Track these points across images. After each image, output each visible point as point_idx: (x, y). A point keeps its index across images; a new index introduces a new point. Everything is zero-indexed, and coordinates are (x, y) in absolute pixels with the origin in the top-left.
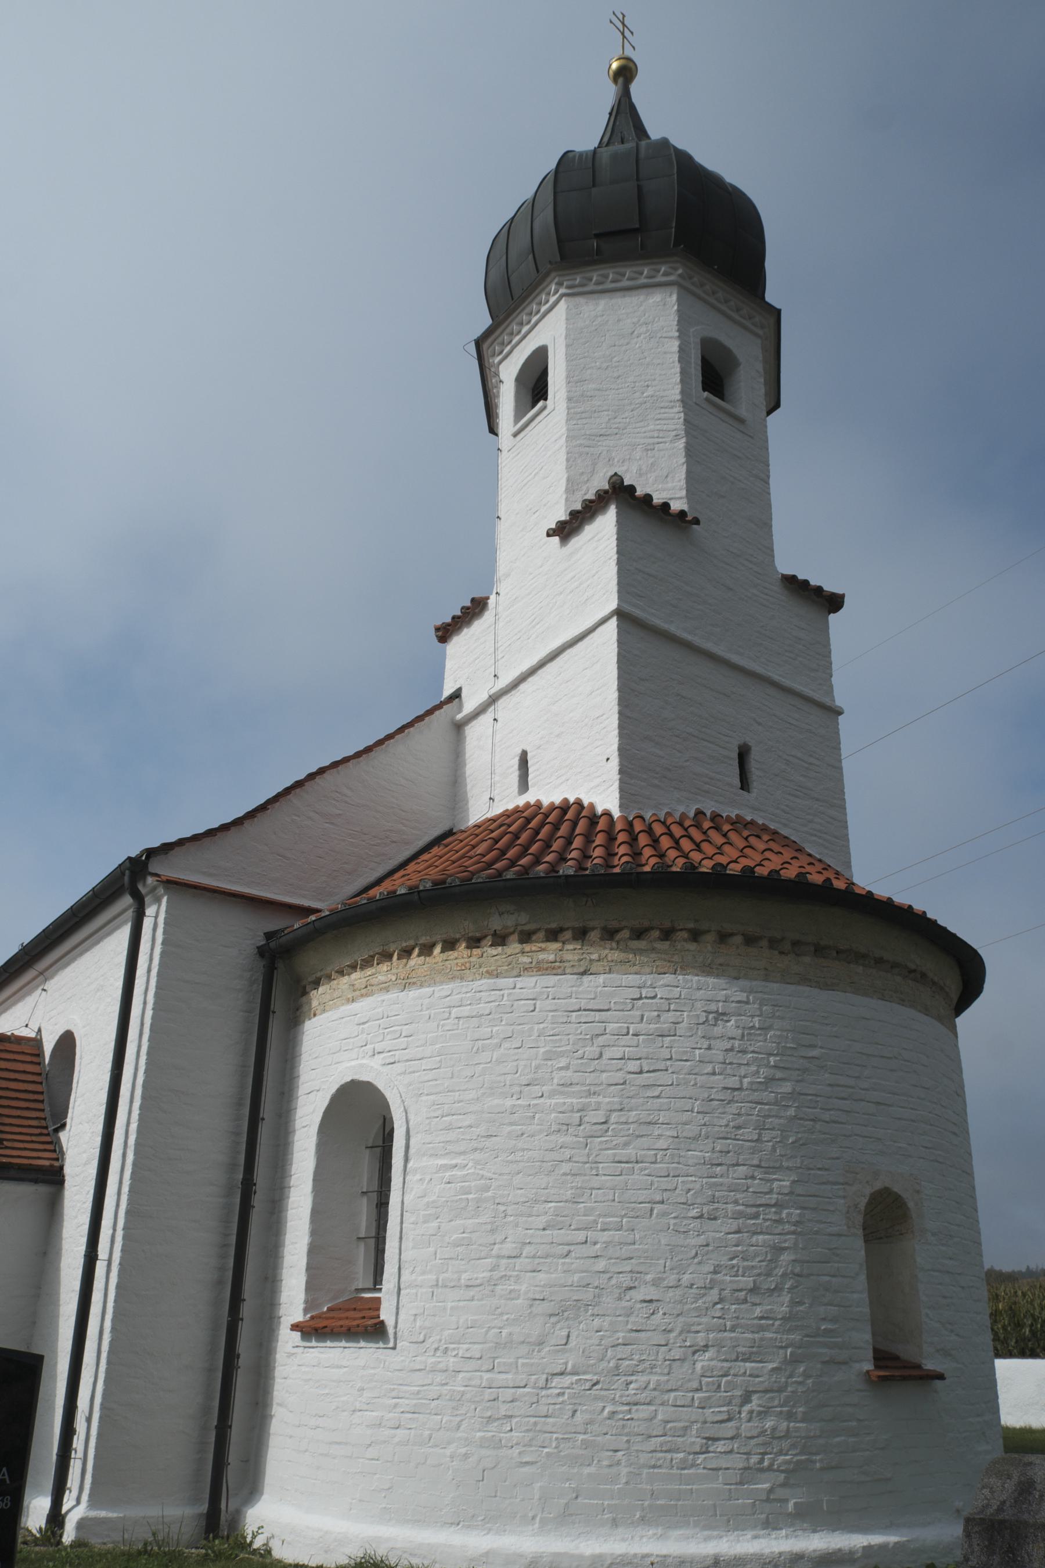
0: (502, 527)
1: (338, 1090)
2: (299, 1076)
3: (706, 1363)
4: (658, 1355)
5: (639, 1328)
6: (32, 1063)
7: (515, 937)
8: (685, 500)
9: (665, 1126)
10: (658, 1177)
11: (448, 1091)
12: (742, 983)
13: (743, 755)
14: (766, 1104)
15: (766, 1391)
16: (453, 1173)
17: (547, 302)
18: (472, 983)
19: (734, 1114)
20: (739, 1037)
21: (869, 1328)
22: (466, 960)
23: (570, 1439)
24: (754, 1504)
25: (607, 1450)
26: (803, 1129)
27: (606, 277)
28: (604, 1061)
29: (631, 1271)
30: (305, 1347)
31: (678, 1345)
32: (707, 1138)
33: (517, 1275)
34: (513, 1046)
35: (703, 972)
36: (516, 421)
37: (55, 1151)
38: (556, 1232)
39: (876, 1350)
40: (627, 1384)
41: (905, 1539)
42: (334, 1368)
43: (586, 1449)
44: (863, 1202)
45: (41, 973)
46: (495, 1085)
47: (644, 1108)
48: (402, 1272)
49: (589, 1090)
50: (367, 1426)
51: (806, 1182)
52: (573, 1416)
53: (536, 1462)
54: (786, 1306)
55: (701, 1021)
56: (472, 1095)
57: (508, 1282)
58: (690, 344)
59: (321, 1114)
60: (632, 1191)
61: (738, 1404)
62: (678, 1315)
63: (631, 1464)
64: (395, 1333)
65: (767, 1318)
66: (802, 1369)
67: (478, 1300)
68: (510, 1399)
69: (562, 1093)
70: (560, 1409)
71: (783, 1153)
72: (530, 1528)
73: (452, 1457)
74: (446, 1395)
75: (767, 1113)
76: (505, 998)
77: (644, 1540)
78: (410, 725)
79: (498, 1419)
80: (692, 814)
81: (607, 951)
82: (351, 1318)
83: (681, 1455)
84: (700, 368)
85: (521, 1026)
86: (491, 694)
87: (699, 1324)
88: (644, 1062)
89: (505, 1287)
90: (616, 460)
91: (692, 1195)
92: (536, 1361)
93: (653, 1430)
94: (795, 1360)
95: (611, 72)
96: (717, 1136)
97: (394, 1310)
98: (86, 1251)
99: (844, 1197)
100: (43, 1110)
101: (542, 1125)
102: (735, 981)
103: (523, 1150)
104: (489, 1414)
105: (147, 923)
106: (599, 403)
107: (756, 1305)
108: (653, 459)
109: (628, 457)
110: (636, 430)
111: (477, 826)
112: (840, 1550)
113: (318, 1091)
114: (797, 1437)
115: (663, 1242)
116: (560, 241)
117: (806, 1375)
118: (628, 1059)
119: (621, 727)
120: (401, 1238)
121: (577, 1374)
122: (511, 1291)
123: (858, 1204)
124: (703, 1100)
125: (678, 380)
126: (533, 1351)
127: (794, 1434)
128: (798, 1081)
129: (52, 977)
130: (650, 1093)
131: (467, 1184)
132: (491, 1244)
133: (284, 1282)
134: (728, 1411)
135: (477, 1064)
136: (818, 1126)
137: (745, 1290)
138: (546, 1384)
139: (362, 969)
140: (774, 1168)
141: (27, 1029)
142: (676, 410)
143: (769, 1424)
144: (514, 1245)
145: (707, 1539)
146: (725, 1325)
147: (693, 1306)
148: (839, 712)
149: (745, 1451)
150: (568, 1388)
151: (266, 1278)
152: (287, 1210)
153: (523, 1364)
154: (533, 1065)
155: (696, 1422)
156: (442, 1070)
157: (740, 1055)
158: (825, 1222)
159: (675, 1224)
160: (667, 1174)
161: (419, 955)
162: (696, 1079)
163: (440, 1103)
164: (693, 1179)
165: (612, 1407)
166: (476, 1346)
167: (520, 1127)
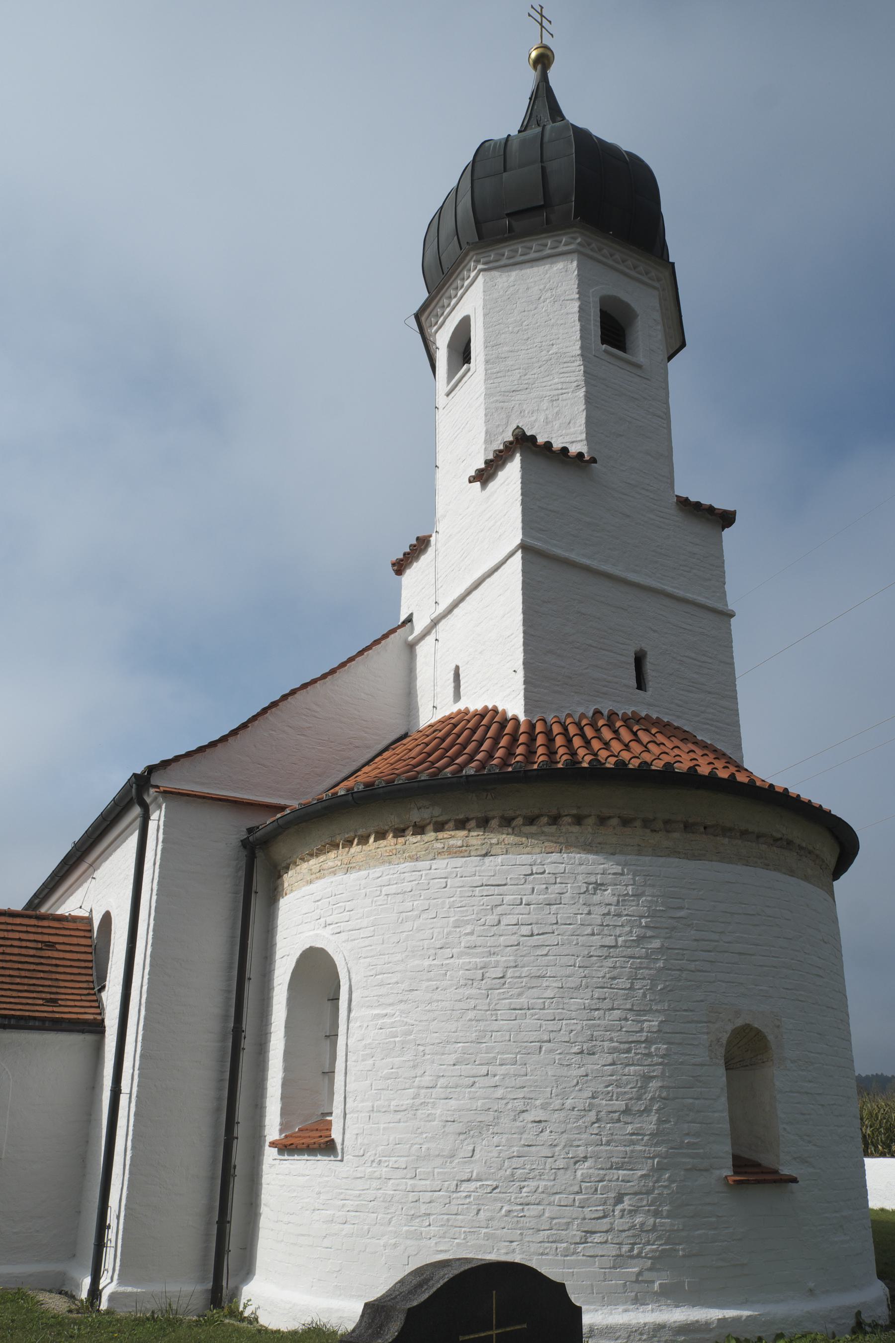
0: (440, 474)
1: (301, 955)
2: (276, 944)
3: (585, 1171)
4: (545, 1165)
5: (530, 1144)
6: (85, 937)
7: (430, 827)
8: (585, 442)
9: (551, 979)
10: (545, 1020)
11: (380, 955)
12: (621, 858)
13: (639, 661)
14: (639, 958)
15: (635, 1194)
16: (385, 1020)
17: (469, 277)
18: (397, 866)
19: (610, 968)
20: (615, 904)
21: (729, 1141)
22: (393, 847)
23: (475, 1232)
24: (625, 1285)
26: (671, 978)
28: (502, 927)
29: (524, 1098)
30: (281, 1160)
31: (562, 1156)
33: (434, 1102)
34: (430, 917)
35: (584, 850)
37: (99, 1007)
38: (464, 1067)
39: (735, 1158)
40: (521, 1188)
41: (757, 1313)
42: (299, 1176)
43: (488, 1240)
44: (725, 1038)
45: (91, 865)
46: (416, 949)
47: (535, 964)
48: (347, 1100)
50: (323, 1222)
51: (673, 1022)
52: (477, 1214)
53: (449, 1251)
54: (655, 1124)
55: (582, 891)
56: (399, 957)
57: (427, 1107)
58: (590, 303)
59: (290, 975)
61: (612, 1204)
62: (562, 1133)
63: (524, 1252)
64: (343, 1149)
65: (637, 1134)
66: (667, 1176)
68: (429, 1201)
69: (468, 954)
70: (467, 1208)
73: (385, 1246)
74: (380, 1198)
75: (638, 966)
76: (423, 878)
78: (368, 648)
80: (590, 714)
81: (504, 836)
82: (312, 1137)
83: (565, 1245)
84: (599, 324)
85: (435, 901)
86: (432, 618)
87: (580, 1140)
88: (535, 927)
89: (424, 1111)
90: (526, 412)
91: (574, 1035)
92: (449, 1170)
93: (542, 1225)
94: (661, 1168)
95: (531, 62)
97: (341, 1130)
98: (112, 1087)
99: (708, 1033)
100: (92, 975)
101: (452, 980)
102: (612, 856)
103: (438, 1001)
104: (412, 1212)
105: (152, 826)
106: (511, 363)
107: (628, 1123)
108: (558, 409)
109: (537, 408)
110: (544, 384)
112: (697, 1321)
113: (288, 955)
114: (663, 1231)
115: (550, 1073)
116: (477, 222)
117: (671, 1180)
118: (522, 925)
119: (525, 644)
120: (346, 1073)
121: (481, 1180)
123: (720, 1038)
124: (584, 957)
125: (579, 337)
126: (446, 1162)
127: (659, 1228)
129: (98, 868)
130: (539, 952)
131: (394, 1029)
132: (413, 1077)
133: (267, 1108)
134: (604, 1210)
135: (401, 932)
136: (684, 975)
137: (619, 1111)
138: (457, 1188)
139: (317, 856)
140: (644, 1010)
141: (81, 910)
143: (638, 1220)
144: (431, 1078)
146: (601, 1140)
147: (575, 1125)
148: (731, 615)
149: (618, 1242)
150: (474, 1192)
151: (256, 1105)
152: (269, 1051)
153: (438, 1173)
154: (445, 931)
155: (576, 1218)
156: (375, 938)
157: (616, 918)
158: (689, 1055)
159: (559, 1059)
160: (553, 1018)
161: (358, 845)
162: (577, 939)
163: (374, 964)
164: (575, 1021)
165: (508, 1206)
166: (402, 1159)
167: (435, 983)
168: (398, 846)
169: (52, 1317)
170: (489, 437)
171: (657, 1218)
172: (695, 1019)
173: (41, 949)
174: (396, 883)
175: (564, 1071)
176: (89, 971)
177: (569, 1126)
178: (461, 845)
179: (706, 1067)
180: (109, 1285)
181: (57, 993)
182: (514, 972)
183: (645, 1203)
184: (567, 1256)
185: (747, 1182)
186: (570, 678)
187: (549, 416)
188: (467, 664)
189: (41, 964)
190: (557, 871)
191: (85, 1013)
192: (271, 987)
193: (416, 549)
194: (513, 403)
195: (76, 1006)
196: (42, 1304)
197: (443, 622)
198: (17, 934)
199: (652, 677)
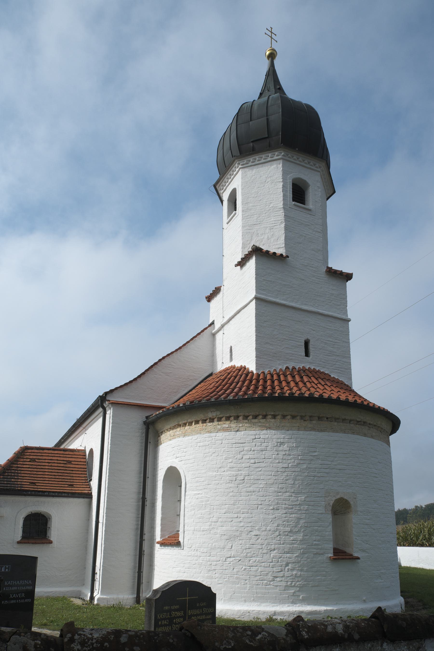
0: (225, 259)
1: (167, 469)
3: (274, 554)
5: (253, 544)
8: (284, 248)
12: (290, 432)
13: (307, 343)
14: (297, 472)
15: (293, 563)
17: (235, 171)
21: (332, 543)
22: (202, 427)
24: (288, 597)
25: (243, 580)
27: (256, 159)
28: (243, 460)
29: (251, 526)
32: (276, 484)
34: (216, 455)
36: (228, 217)
37: (90, 487)
38: (228, 514)
40: (249, 560)
43: (237, 579)
48: (185, 526)
49: (239, 469)
50: (177, 572)
52: (233, 570)
55: (275, 445)
56: (204, 471)
60: (251, 501)
62: (266, 540)
64: (183, 545)
65: (295, 540)
67: (206, 535)
69: (230, 470)
70: (229, 568)
71: (302, 488)
72: (221, 602)
75: (297, 475)
77: (254, 606)
79: (212, 570)
80: (284, 369)
84: (291, 192)
85: (218, 449)
87: (272, 542)
90: (260, 234)
91: (271, 502)
92: (223, 553)
94: (304, 553)
96: (279, 483)
97: (183, 538)
99: (325, 501)
100: (86, 474)
103: (219, 489)
104: (209, 569)
105: (108, 416)
109: (264, 232)
111: (220, 372)
112: (316, 611)
114: (304, 577)
115: (261, 517)
116: (239, 145)
117: (308, 558)
119: (256, 340)
120: (184, 516)
122: (215, 532)
123: (330, 503)
125: (282, 199)
126: (222, 550)
128: (308, 464)
129: (87, 429)
130: (258, 470)
134: (281, 569)
136: (315, 478)
139: (173, 430)
142: (281, 212)
143: (294, 573)
144: (216, 518)
145: (273, 606)
150: (232, 561)
151: (152, 527)
153: (219, 554)
154: (222, 461)
157: (288, 456)
158: (316, 510)
159: (265, 511)
161: (188, 426)
164: (271, 497)
167: (217, 481)
168: (203, 427)
169: (77, 606)
170: (244, 246)
171: (302, 572)
172: (320, 496)
173: (66, 464)
174: (203, 442)
175: (267, 516)
176: (85, 473)
177: (268, 537)
178: (228, 427)
179: (323, 515)
180: (97, 595)
181: (73, 482)
182: (248, 477)
183: (297, 566)
184: (267, 586)
185: (338, 559)
186: (276, 353)
187: (269, 236)
188: (235, 346)
189: (66, 470)
190: (265, 438)
191: (85, 490)
192: (157, 481)
193: (215, 292)
194: (254, 230)
195: (81, 487)
196: (73, 602)
197: (226, 326)
198: (56, 457)
199: (312, 351)
